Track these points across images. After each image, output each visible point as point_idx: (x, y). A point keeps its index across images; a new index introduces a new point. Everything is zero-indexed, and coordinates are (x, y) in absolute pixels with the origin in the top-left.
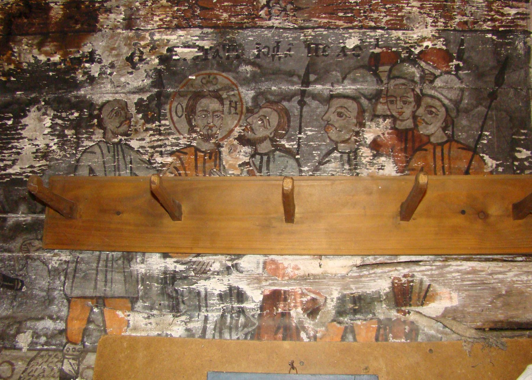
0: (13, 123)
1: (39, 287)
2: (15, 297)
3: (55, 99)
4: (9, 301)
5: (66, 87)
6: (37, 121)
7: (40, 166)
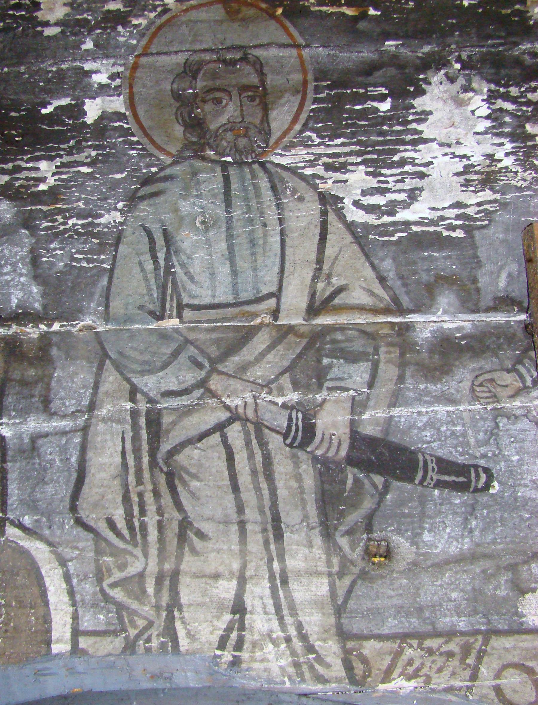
0: (393, 107)
1: (533, 481)
2: (472, 510)
3: (484, 59)
4: (459, 519)
5: (503, 34)
6: (451, 106)
7: (479, 204)
